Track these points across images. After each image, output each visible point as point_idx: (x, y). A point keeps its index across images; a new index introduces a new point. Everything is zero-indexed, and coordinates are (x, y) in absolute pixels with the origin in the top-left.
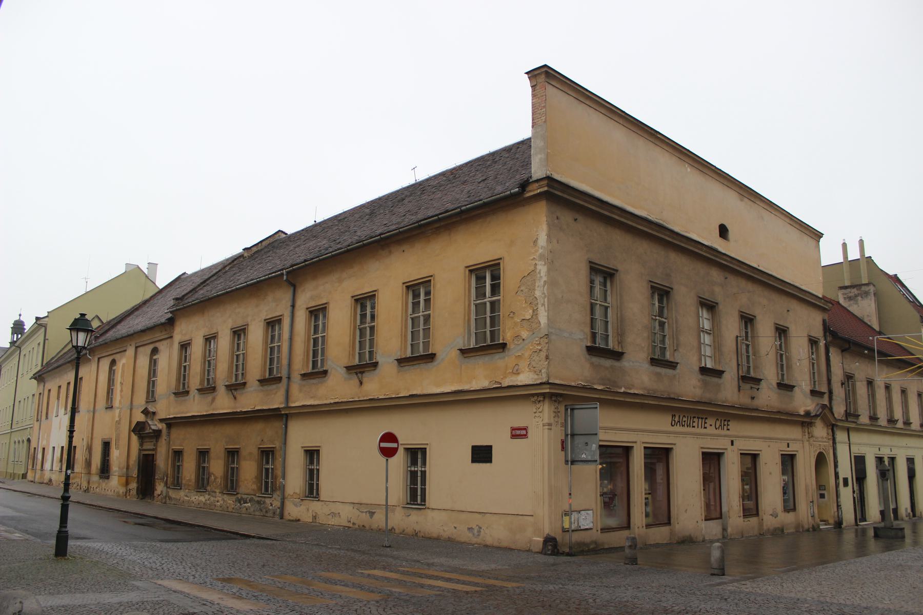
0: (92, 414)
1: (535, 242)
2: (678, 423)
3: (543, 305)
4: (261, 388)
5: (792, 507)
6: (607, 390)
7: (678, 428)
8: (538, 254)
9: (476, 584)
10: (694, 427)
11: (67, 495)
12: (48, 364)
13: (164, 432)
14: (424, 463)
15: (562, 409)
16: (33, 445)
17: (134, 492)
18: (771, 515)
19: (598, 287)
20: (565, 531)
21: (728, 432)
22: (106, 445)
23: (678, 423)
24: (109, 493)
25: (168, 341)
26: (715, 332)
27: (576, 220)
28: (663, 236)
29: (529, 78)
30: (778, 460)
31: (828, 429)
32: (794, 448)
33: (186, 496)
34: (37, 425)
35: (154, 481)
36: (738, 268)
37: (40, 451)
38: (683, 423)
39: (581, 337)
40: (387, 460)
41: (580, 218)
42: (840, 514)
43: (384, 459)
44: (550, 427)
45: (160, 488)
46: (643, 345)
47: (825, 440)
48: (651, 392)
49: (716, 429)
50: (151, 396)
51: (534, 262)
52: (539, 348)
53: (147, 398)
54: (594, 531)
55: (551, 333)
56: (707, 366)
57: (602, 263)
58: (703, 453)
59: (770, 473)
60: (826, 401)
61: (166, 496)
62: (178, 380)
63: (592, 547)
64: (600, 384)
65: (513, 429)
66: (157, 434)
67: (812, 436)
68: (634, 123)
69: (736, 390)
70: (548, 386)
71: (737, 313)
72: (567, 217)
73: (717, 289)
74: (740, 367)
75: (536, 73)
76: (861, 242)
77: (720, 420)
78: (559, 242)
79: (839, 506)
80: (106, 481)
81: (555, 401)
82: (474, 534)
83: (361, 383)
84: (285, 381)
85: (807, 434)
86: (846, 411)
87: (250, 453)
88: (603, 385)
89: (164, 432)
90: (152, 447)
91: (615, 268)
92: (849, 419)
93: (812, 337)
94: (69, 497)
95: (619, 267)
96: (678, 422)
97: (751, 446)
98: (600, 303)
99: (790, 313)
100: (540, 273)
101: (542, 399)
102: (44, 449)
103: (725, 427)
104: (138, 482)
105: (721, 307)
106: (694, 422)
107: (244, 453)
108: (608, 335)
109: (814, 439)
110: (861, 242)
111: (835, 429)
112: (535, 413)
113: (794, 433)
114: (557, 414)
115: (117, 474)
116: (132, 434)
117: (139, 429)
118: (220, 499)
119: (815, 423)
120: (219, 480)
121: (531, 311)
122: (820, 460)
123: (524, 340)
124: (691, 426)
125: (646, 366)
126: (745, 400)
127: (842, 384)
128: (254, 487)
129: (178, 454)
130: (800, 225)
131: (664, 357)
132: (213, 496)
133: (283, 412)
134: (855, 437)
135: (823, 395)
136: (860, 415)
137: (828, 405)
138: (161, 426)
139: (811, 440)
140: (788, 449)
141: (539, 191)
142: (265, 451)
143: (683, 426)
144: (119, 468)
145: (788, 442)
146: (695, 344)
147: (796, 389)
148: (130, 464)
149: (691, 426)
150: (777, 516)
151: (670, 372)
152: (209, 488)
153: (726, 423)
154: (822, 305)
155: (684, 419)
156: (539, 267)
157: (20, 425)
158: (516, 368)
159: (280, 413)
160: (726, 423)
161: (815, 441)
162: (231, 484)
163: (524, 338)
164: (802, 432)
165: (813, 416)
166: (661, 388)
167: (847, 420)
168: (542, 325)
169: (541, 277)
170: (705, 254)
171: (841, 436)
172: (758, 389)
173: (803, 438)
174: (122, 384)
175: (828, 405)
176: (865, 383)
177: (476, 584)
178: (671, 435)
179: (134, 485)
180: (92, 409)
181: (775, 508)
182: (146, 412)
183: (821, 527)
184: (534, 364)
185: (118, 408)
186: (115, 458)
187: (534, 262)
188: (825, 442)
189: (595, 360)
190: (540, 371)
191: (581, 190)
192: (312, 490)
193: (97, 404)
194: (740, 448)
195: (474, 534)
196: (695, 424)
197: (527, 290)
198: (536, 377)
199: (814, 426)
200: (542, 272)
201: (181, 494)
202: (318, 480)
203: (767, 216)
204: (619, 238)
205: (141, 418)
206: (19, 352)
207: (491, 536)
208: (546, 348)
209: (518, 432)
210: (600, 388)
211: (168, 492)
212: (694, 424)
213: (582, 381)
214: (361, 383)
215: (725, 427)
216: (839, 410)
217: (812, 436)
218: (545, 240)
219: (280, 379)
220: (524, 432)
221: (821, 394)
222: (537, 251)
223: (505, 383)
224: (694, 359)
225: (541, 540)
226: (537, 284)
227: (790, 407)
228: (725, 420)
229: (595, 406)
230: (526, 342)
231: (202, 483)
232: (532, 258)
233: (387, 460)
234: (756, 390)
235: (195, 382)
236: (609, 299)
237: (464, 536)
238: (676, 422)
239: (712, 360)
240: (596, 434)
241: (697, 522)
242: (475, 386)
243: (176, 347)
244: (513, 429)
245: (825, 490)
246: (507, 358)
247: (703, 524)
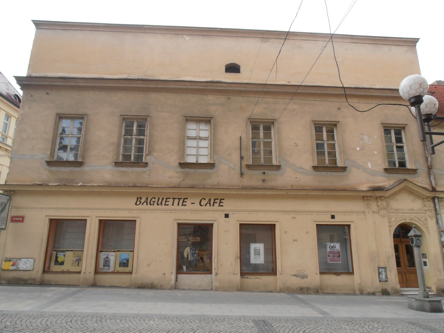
5: (351, 271)
18: (295, 275)
27: (48, 94)
38: (152, 203)
41: (49, 92)
57: (322, 120)
68: (340, 37)
91: (210, 116)
93: (188, 117)
130: (351, 38)
131: (336, 165)
135: (346, 168)
150: (307, 277)
170: (190, 87)
178: (187, 212)
183: (414, 300)
188: (422, 213)
189: (54, 169)
203: (307, 45)
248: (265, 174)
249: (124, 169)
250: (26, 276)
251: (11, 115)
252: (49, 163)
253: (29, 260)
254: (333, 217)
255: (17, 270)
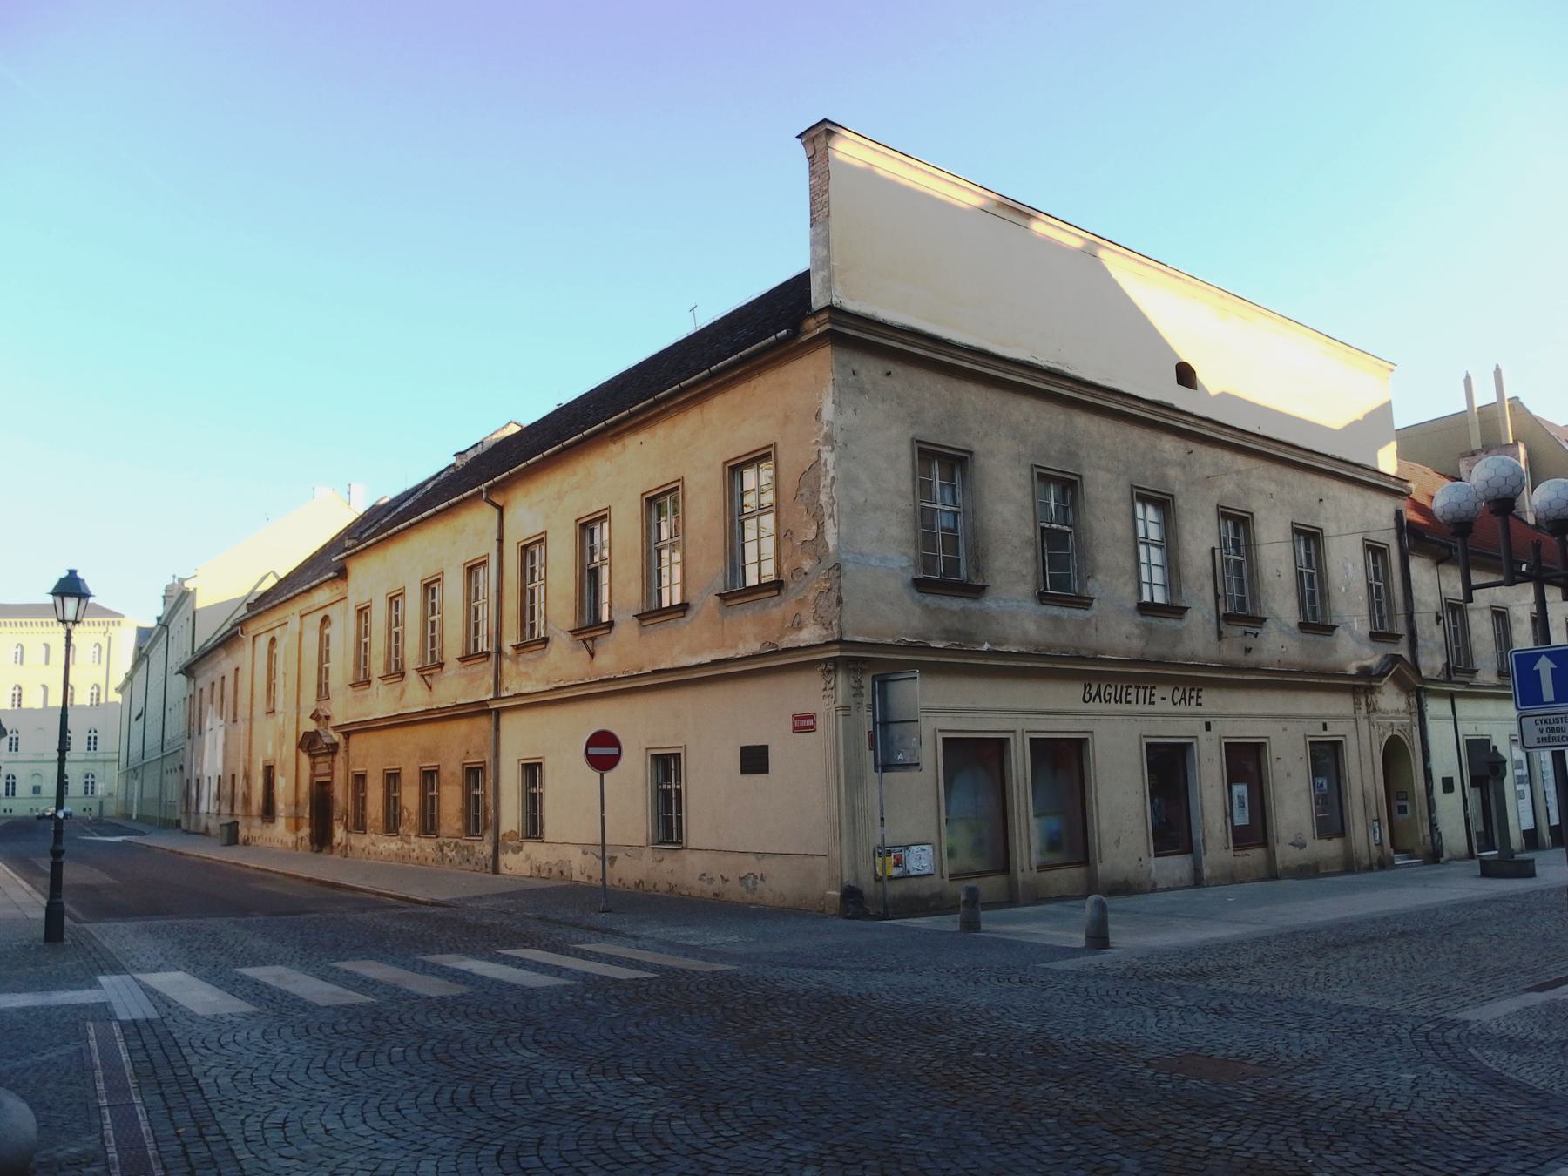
0: (248, 723)
1: (818, 415)
2: (1098, 698)
3: (831, 516)
4: (463, 670)
6: (955, 648)
7: (1097, 706)
8: (822, 434)
9: (639, 965)
10: (1129, 702)
11: (60, 848)
12: (199, 654)
13: (342, 745)
14: (678, 780)
15: (867, 682)
16: (186, 776)
17: (307, 842)
18: (1292, 844)
19: (938, 481)
20: (878, 879)
21: (1199, 709)
22: (269, 771)
23: (1098, 698)
24: (276, 844)
25: (343, 602)
26: (1170, 543)
28: (1059, 390)
29: (804, 144)
30: (1303, 751)
31: (1408, 696)
32: (1336, 730)
33: (373, 844)
34: (188, 743)
35: (332, 822)
36: (1214, 435)
37: (193, 782)
38: (1107, 698)
39: (903, 565)
40: (602, 775)
42: (1436, 837)
43: (597, 775)
44: (846, 713)
45: (339, 834)
46: (1024, 573)
47: (1404, 715)
48: (1041, 648)
49: (1175, 704)
50: (323, 692)
51: (817, 448)
52: (828, 585)
53: (319, 695)
54: (937, 877)
55: (846, 560)
56: (1156, 601)
58: (1149, 746)
59: (1288, 775)
60: (1402, 650)
61: (346, 846)
62: (357, 666)
63: (932, 904)
64: (942, 640)
65: (796, 718)
66: (333, 749)
67: (1375, 710)
69: (1214, 637)
70: (838, 647)
71: (1214, 509)
72: (870, 369)
73: (1173, 473)
74: (1221, 600)
75: (813, 133)
76: (1498, 373)
77: (1181, 690)
78: (858, 412)
79: (1433, 826)
80: (271, 825)
81: (855, 670)
82: (747, 887)
83: (592, 655)
84: (493, 656)
85: (1363, 706)
86: (1447, 664)
87: (453, 774)
88: (947, 640)
89: (342, 745)
90: (327, 771)
92: (1454, 679)
94: (63, 852)
95: (976, 447)
96: (1097, 695)
97: (1247, 731)
98: (941, 507)
99: (1325, 502)
100: (825, 464)
101: (831, 667)
102: (198, 780)
103: (1193, 701)
104: (311, 826)
105: (1180, 502)
106: (1128, 694)
107: (444, 773)
108: (959, 559)
109: (1380, 714)
110: (1498, 373)
111: (1422, 695)
112: (825, 689)
113: (1340, 705)
114: (857, 691)
115: (282, 814)
116: (301, 753)
117: (308, 743)
118: (416, 846)
119: (1380, 687)
120: (413, 817)
121: (815, 527)
122: (1394, 752)
123: (806, 574)
124: (1124, 701)
125: (1031, 606)
126: (1230, 652)
127: (1438, 619)
128: (459, 825)
129: (360, 779)
132: (406, 842)
133: (491, 707)
134: (1466, 708)
136: (1477, 671)
137: (1408, 658)
138: (337, 737)
139: (1374, 716)
140: (1325, 733)
141: (818, 331)
142: (472, 768)
143: (1106, 701)
144: (286, 805)
145: (1208, 719)
146: (1129, 564)
147: (1340, 631)
148: (301, 800)
149: (1124, 701)
150: (1305, 846)
151: (1079, 614)
152: (401, 830)
153: (1194, 694)
154: (1393, 487)
155: (1109, 690)
156: (824, 456)
157: (172, 745)
158: (797, 620)
159: (486, 708)
160: (1194, 694)
161: (1378, 718)
162: (429, 824)
163: (806, 570)
164: (1355, 703)
165: (1376, 676)
166: (1063, 639)
167: (1449, 680)
168: (831, 549)
169: (827, 471)
170: (1143, 414)
171: (1436, 708)
172: (1256, 635)
173: (1355, 713)
174: (285, 674)
175: (1408, 658)
176: (1488, 614)
177: (639, 965)
179: (305, 831)
180: (248, 717)
181: (1300, 833)
182: (316, 716)
183: (1397, 863)
184: (820, 611)
185: (281, 713)
186: (281, 791)
187: (817, 448)
189: (931, 600)
190: (831, 623)
191: (895, 324)
192: (533, 827)
193: (254, 708)
194: (1223, 734)
195: (747, 887)
196: (1132, 698)
197: (808, 493)
198: (825, 632)
199: (1380, 692)
200: (828, 463)
201: (360, 842)
202: (679, 810)
204: (974, 398)
205: (310, 726)
206: (165, 634)
207: (771, 890)
208: (837, 586)
209: (803, 723)
210: (941, 646)
211: (348, 839)
212: (1129, 698)
213: (906, 635)
214: (592, 655)
215: (1193, 701)
216: (1432, 662)
217: (1375, 710)
218: (832, 411)
219: (488, 654)
220: (810, 722)
221: (1394, 638)
222: (821, 429)
223: (785, 643)
224: (1130, 589)
225: (837, 893)
226: (822, 484)
227: (1328, 662)
228: (1191, 690)
229: (913, 675)
230: (809, 577)
231: (392, 825)
232: (813, 441)
233: (602, 775)
234: (1253, 636)
235: (377, 667)
236: (959, 500)
237: (735, 891)
238: (1093, 695)
239: (1165, 591)
240: (917, 721)
241: (1140, 859)
242: (743, 650)
243: (352, 613)
244: (796, 718)
245: (1406, 799)
246: (783, 604)
247: (1154, 862)
248: (1250, 649)
249: (1055, 611)
250: (923, 888)
251: (1141, 747)
252: (919, 585)
253: (924, 847)
254: (1325, 727)
255: (906, 876)
